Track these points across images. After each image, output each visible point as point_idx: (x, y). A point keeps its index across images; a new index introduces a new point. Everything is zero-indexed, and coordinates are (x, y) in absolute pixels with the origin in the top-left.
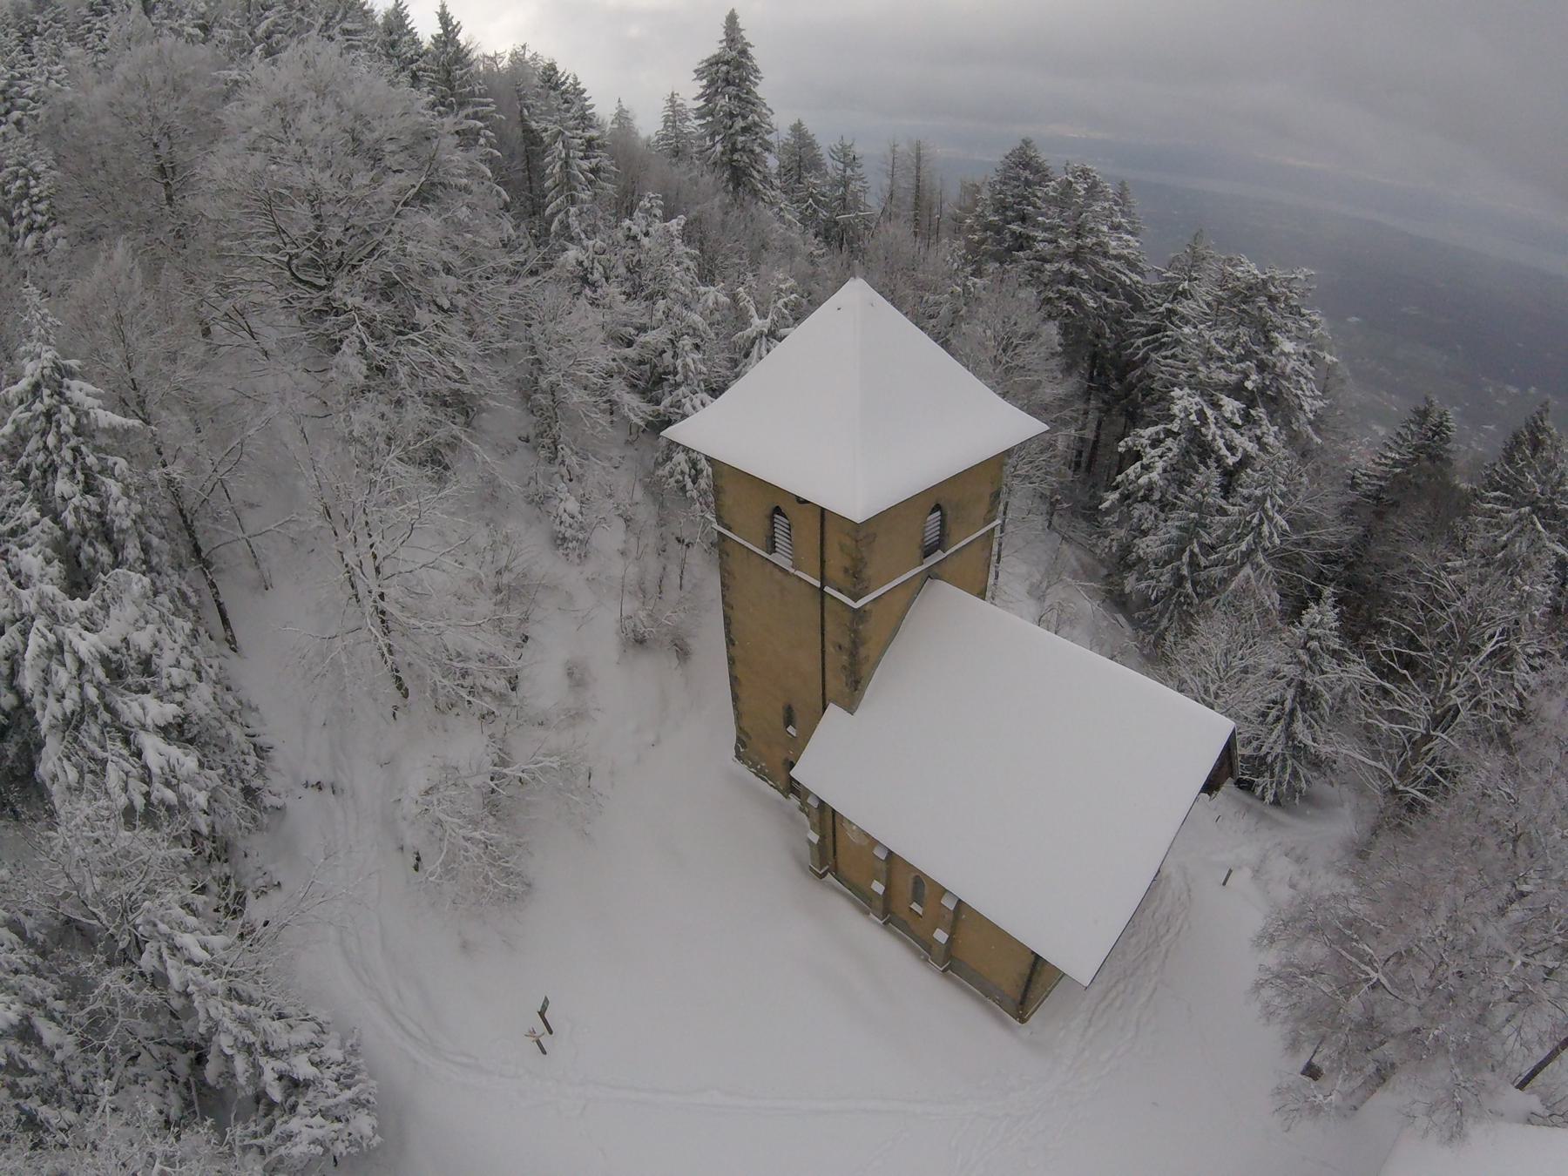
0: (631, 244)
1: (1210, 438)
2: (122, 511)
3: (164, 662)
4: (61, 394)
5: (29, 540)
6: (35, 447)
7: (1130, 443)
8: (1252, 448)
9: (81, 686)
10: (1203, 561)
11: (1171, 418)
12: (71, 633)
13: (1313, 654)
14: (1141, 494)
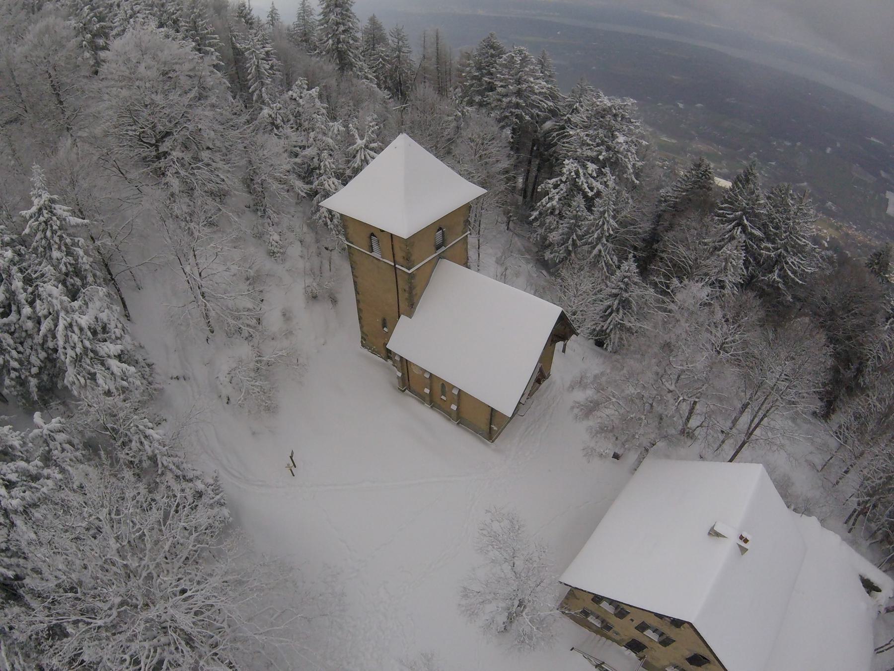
0: (293, 102)
1: (580, 183)
2: (85, 261)
3: (111, 326)
4: (51, 212)
5: (46, 279)
6: (40, 237)
7: (543, 187)
8: (601, 187)
9: (82, 341)
10: (578, 243)
11: (562, 174)
12: (76, 316)
13: (627, 284)
14: (549, 211)
